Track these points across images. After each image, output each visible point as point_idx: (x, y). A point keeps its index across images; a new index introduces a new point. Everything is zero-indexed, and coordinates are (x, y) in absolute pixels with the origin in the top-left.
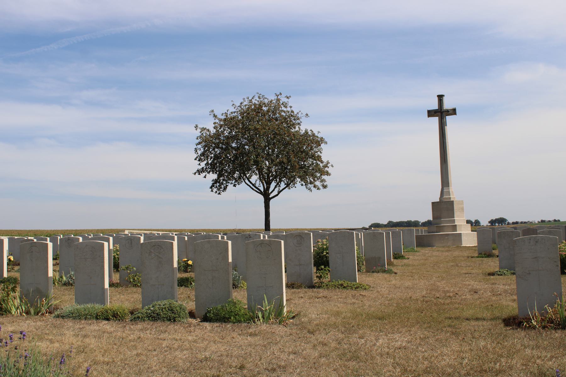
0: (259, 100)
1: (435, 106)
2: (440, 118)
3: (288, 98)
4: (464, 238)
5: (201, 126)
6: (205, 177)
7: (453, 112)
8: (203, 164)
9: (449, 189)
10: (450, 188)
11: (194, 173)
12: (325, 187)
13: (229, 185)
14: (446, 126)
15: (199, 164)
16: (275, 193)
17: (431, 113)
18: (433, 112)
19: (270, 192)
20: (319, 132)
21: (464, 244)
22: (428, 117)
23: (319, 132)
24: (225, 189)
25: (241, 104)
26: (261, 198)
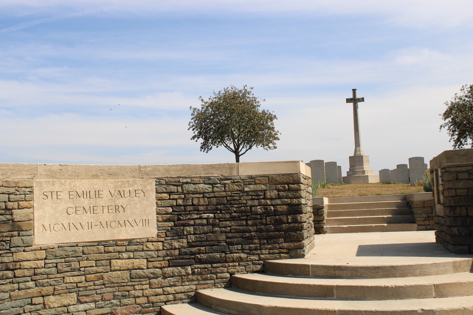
0: (231, 90)
1: (351, 97)
2: (354, 104)
3: (252, 88)
4: (369, 178)
5: (193, 107)
7: (363, 100)
9: (360, 148)
10: (360, 147)
11: (191, 138)
14: (358, 108)
15: (194, 133)
17: (348, 101)
18: (350, 100)
19: (239, 151)
20: (273, 112)
21: (370, 182)
22: (347, 103)
23: (273, 112)
24: (211, 149)
25: (219, 92)
26: (234, 155)
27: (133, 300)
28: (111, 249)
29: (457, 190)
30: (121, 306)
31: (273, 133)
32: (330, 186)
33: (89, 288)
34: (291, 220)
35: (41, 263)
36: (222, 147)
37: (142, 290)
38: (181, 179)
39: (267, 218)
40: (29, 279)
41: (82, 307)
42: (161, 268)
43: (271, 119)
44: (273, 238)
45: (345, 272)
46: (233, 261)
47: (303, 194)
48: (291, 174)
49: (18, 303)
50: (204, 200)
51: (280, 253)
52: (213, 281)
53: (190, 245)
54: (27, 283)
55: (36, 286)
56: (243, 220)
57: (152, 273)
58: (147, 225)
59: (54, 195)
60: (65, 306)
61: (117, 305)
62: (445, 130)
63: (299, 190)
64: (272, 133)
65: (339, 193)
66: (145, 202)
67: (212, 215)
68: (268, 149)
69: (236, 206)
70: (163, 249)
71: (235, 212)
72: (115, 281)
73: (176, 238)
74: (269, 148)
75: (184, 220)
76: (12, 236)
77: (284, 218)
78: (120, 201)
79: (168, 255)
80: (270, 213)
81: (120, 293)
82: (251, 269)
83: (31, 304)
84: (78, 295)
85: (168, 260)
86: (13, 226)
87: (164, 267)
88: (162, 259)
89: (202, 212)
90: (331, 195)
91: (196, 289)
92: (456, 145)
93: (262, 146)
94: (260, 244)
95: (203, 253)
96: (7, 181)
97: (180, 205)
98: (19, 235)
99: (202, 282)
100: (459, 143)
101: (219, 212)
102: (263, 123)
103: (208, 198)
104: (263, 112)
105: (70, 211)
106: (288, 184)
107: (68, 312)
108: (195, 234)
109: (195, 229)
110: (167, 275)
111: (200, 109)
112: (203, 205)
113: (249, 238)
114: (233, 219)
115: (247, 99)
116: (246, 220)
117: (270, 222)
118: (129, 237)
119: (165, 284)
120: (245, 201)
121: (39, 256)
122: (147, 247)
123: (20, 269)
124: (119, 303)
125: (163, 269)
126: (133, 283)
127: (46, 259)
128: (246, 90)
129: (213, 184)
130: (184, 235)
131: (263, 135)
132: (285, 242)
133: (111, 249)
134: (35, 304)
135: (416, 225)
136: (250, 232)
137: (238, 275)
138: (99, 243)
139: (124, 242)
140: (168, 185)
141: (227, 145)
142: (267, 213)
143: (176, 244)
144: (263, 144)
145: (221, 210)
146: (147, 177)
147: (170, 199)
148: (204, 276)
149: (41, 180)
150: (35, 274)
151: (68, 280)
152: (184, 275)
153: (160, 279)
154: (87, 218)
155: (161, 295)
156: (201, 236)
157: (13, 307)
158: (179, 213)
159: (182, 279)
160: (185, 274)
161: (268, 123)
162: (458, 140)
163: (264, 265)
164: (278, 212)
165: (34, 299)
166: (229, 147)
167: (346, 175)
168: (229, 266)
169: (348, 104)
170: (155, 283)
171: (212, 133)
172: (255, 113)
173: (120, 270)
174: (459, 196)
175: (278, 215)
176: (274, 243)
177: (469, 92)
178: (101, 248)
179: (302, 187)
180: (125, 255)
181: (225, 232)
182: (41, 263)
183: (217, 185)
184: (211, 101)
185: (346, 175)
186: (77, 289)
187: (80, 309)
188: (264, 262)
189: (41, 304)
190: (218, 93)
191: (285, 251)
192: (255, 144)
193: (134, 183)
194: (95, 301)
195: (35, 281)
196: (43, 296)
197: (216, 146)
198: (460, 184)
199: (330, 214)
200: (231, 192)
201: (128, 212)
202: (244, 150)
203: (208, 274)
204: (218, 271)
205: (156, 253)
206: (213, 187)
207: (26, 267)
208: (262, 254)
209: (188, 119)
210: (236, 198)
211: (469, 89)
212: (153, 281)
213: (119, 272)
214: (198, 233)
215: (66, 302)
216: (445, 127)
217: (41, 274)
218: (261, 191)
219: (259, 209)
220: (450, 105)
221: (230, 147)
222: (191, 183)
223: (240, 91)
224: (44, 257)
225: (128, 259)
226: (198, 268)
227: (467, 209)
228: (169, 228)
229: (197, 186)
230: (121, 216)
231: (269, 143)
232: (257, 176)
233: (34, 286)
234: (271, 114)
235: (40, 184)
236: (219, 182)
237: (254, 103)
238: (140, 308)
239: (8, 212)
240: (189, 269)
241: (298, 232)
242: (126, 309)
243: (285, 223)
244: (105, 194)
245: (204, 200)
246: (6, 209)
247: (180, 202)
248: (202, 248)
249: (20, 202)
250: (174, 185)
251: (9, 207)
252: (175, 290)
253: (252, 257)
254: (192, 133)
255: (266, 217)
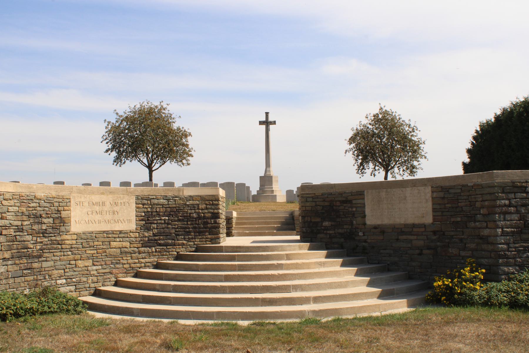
1: (264, 119)
3: (168, 105)
5: (107, 120)
7: (274, 123)
12: (188, 164)
15: (108, 146)
17: (261, 123)
20: (188, 129)
21: (278, 201)
23: (188, 129)
24: (124, 163)
25: (135, 106)
26: (147, 170)
27: (122, 265)
28: (110, 236)
29: (306, 207)
30: (115, 269)
31: (188, 150)
32: (239, 204)
33: (99, 257)
34: (213, 222)
35: (74, 242)
36: (135, 162)
37: (127, 260)
38: (150, 196)
39: (199, 220)
40: (68, 250)
41: (95, 268)
42: (138, 248)
43: (186, 136)
44: (202, 232)
45: (242, 249)
46: (179, 245)
47: (221, 207)
48: (214, 195)
49: (63, 263)
50: (163, 209)
51: (206, 241)
52: (167, 257)
53: (154, 235)
54: (68, 252)
55: (72, 254)
56: (185, 221)
57: (133, 251)
58: (130, 223)
59: (80, 203)
60: (86, 267)
61: (113, 268)
62: (350, 154)
63: (218, 205)
64: (186, 150)
65: (245, 209)
66: (129, 209)
67: (167, 218)
68: (182, 165)
69: (181, 213)
70: (139, 237)
71: (181, 216)
72: (112, 254)
73: (146, 230)
74: (183, 164)
75: (151, 220)
76: (60, 226)
77: (209, 221)
78: (116, 208)
79: (141, 241)
80: (201, 217)
81: (115, 261)
82: (189, 250)
83: (70, 264)
84: (93, 261)
85: (142, 243)
86: (61, 220)
87: (139, 247)
88: (138, 242)
89: (162, 216)
90: (239, 210)
91: (157, 261)
92: (359, 169)
93: (176, 162)
94: (195, 236)
95: (162, 240)
96: (58, 195)
97: (149, 212)
98: (64, 226)
99: (160, 257)
100: (362, 167)
101: (171, 216)
102: (178, 140)
103: (165, 208)
104: (179, 129)
105: (89, 213)
106: (212, 201)
107: (88, 270)
108: (157, 229)
109: (157, 226)
110: (141, 252)
111: (114, 122)
112: (162, 212)
113: (188, 232)
114: (179, 220)
115: (163, 115)
116: (187, 221)
117: (201, 223)
118: (120, 229)
119: (140, 257)
120: (187, 210)
121: (73, 238)
122: (130, 235)
123: (64, 244)
124: (114, 267)
125: (139, 249)
126: (122, 256)
127: (76, 240)
128: (162, 106)
129: (168, 200)
130: (151, 229)
131: (177, 151)
132: (209, 235)
133: (110, 236)
134: (72, 265)
135: (295, 232)
136: (189, 228)
137: (181, 253)
138: (104, 232)
139: (118, 232)
140: (143, 199)
141: (140, 159)
142: (199, 218)
143: (146, 234)
144: (176, 160)
145: (172, 215)
146: (131, 195)
147: (143, 208)
148: (162, 253)
149: (75, 195)
150: (72, 248)
151: (88, 252)
152: (151, 253)
153: (137, 254)
154: (98, 217)
155: (137, 263)
156: (161, 230)
157: (61, 265)
158: (148, 216)
159: (149, 254)
160: (151, 252)
161: (182, 140)
162: (361, 164)
163: (196, 248)
164: (206, 217)
165: (71, 262)
166: (142, 162)
167: (256, 193)
168: (176, 248)
169: (261, 126)
170: (134, 256)
171: (125, 147)
172: (171, 130)
173: (115, 248)
174: (307, 210)
175: (206, 219)
176: (203, 235)
177: (372, 121)
178: (105, 235)
179: (220, 203)
180: (118, 240)
181: (175, 228)
182: (74, 242)
183: (171, 201)
184: (126, 115)
185: (256, 193)
186: (92, 258)
187: (94, 269)
188: (197, 246)
189: (73, 264)
190: (134, 107)
191: (209, 240)
192: (169, 159)
193: (124, 197)
194: (102, 265)
195: (71, 251)
196: (75, 260)
197: (129, 161)
198: (308, 204)
199: (237, 224)
200: (179, 204)
201: (120, 214)
202: (157, 166)
203: (164, 252)
204: (170, 250)
205: (135, 239)
206: (168, 202)
207: (67, 243)
208: (196, 242)
209: (101, 130)
210: (181, 208)
211: (373, 118)
212: (133, 255)
213: (114, 249)
214: (159, 228)
215: (87, 264)
216: (350, 152)
217: (74, 248)
218: (196, 205)
219: (195, 215)
220: (355, 131)
221: (143, 161)
222: (155, 199)
223: (156, 107)
224: (76, 238)
225: (119, 242)
226: (159, 248)
227: (311, 218)
228: (143, 225)
229: (159, 201)
230: (116, 217)
231: (182, 160)
232: (194, 196)
233: (71, 254)
234: (186, 131)
235: (74, 197)
236: (172, 199)
237: (170, 120)
238: (125, 270)
239: (59, 213)
240: (154, 249)
241: (217, 229)
242: (117, 270)
243: (209, 224)
244: (107, 203)
245: (163, 209)
246: (58, 211)
247: (149, 210)
248: (161, 237)
249: (65, 207)
250: (146, 200)
251: (59, 210)
252: (145, 261)
253: (190, 243)
254: (105, 146)
255: (199, 220)
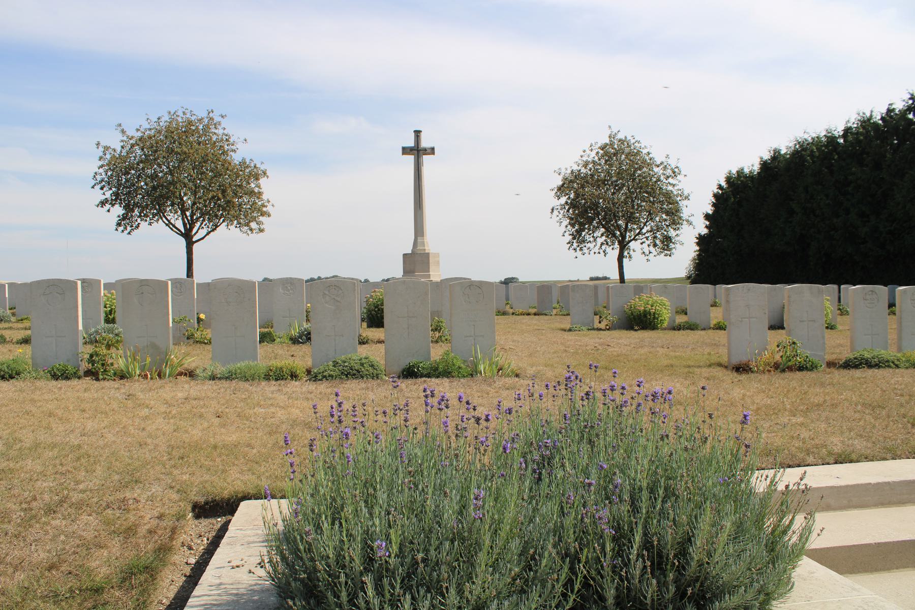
0: (183, 116)
1: (411, 143)
3: (222, 117)
6: (109, 211)
7: (432, 151)
8: (108, 194)
10: (425, 238)
12: (261, 230)
13: (142, 223)
15: (104, 194)
16: (202, 233)
17: (406, 151)
20: (262, 163)
24: (138, 227)
26: (182, 242)
